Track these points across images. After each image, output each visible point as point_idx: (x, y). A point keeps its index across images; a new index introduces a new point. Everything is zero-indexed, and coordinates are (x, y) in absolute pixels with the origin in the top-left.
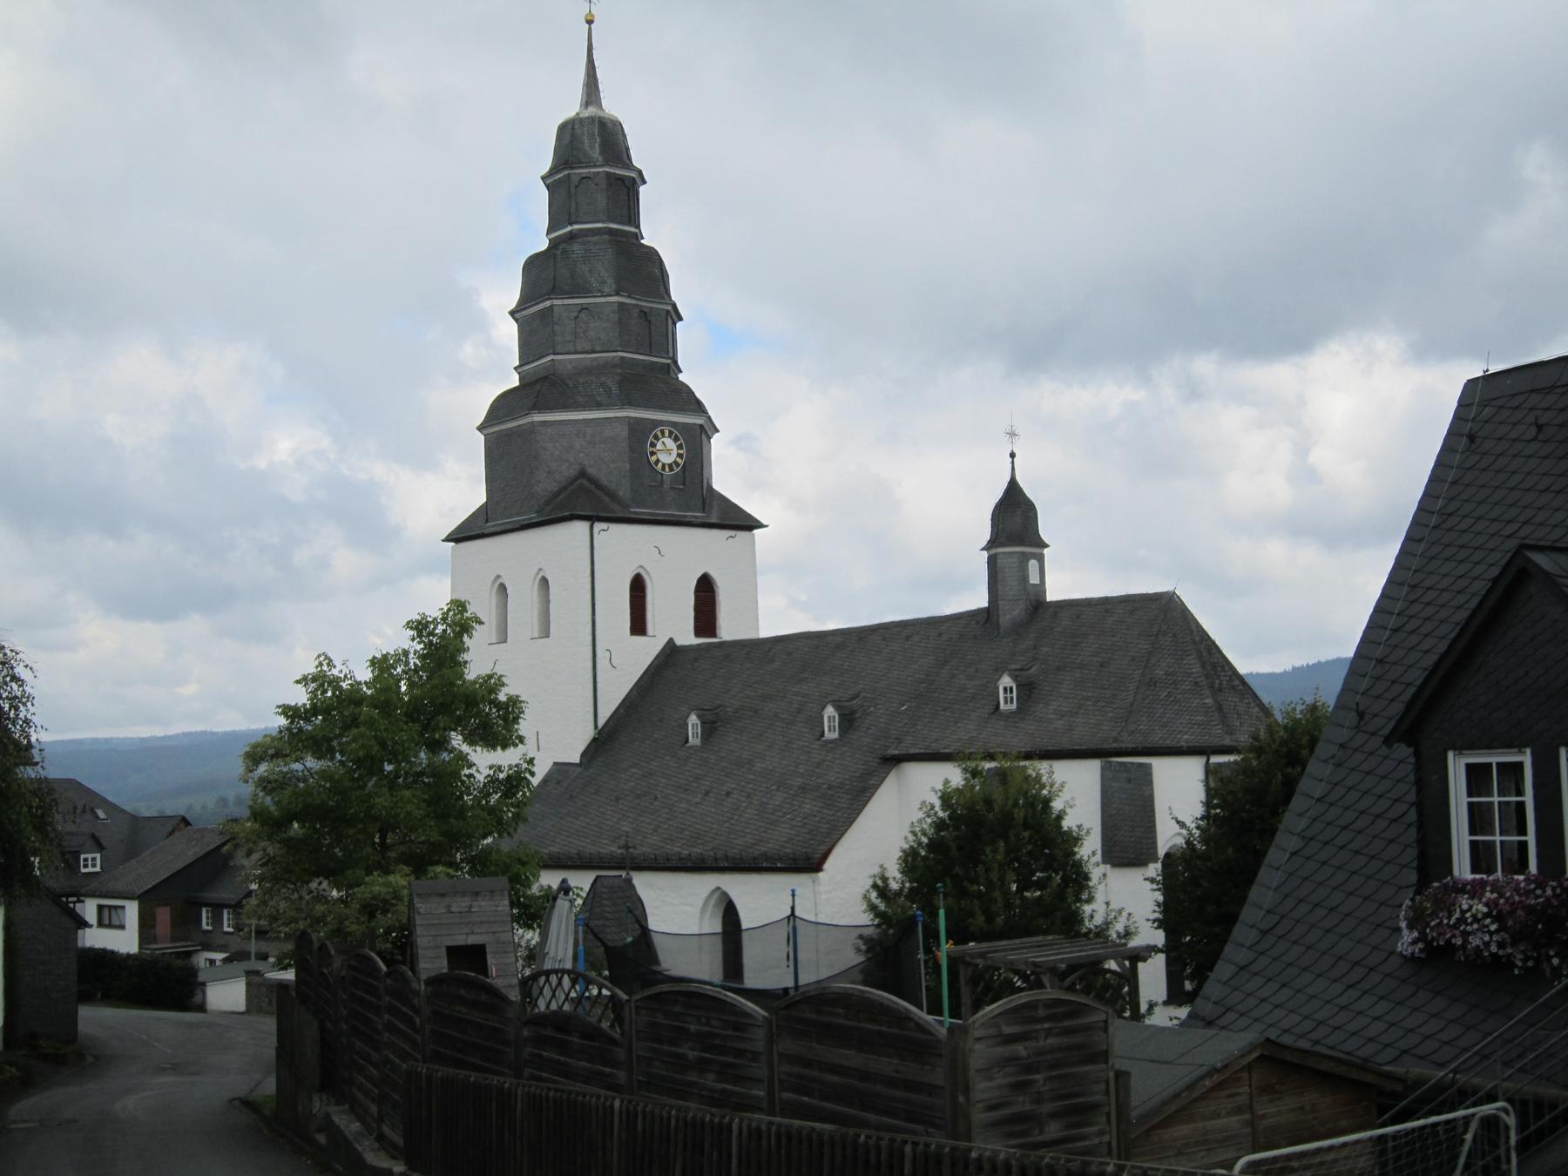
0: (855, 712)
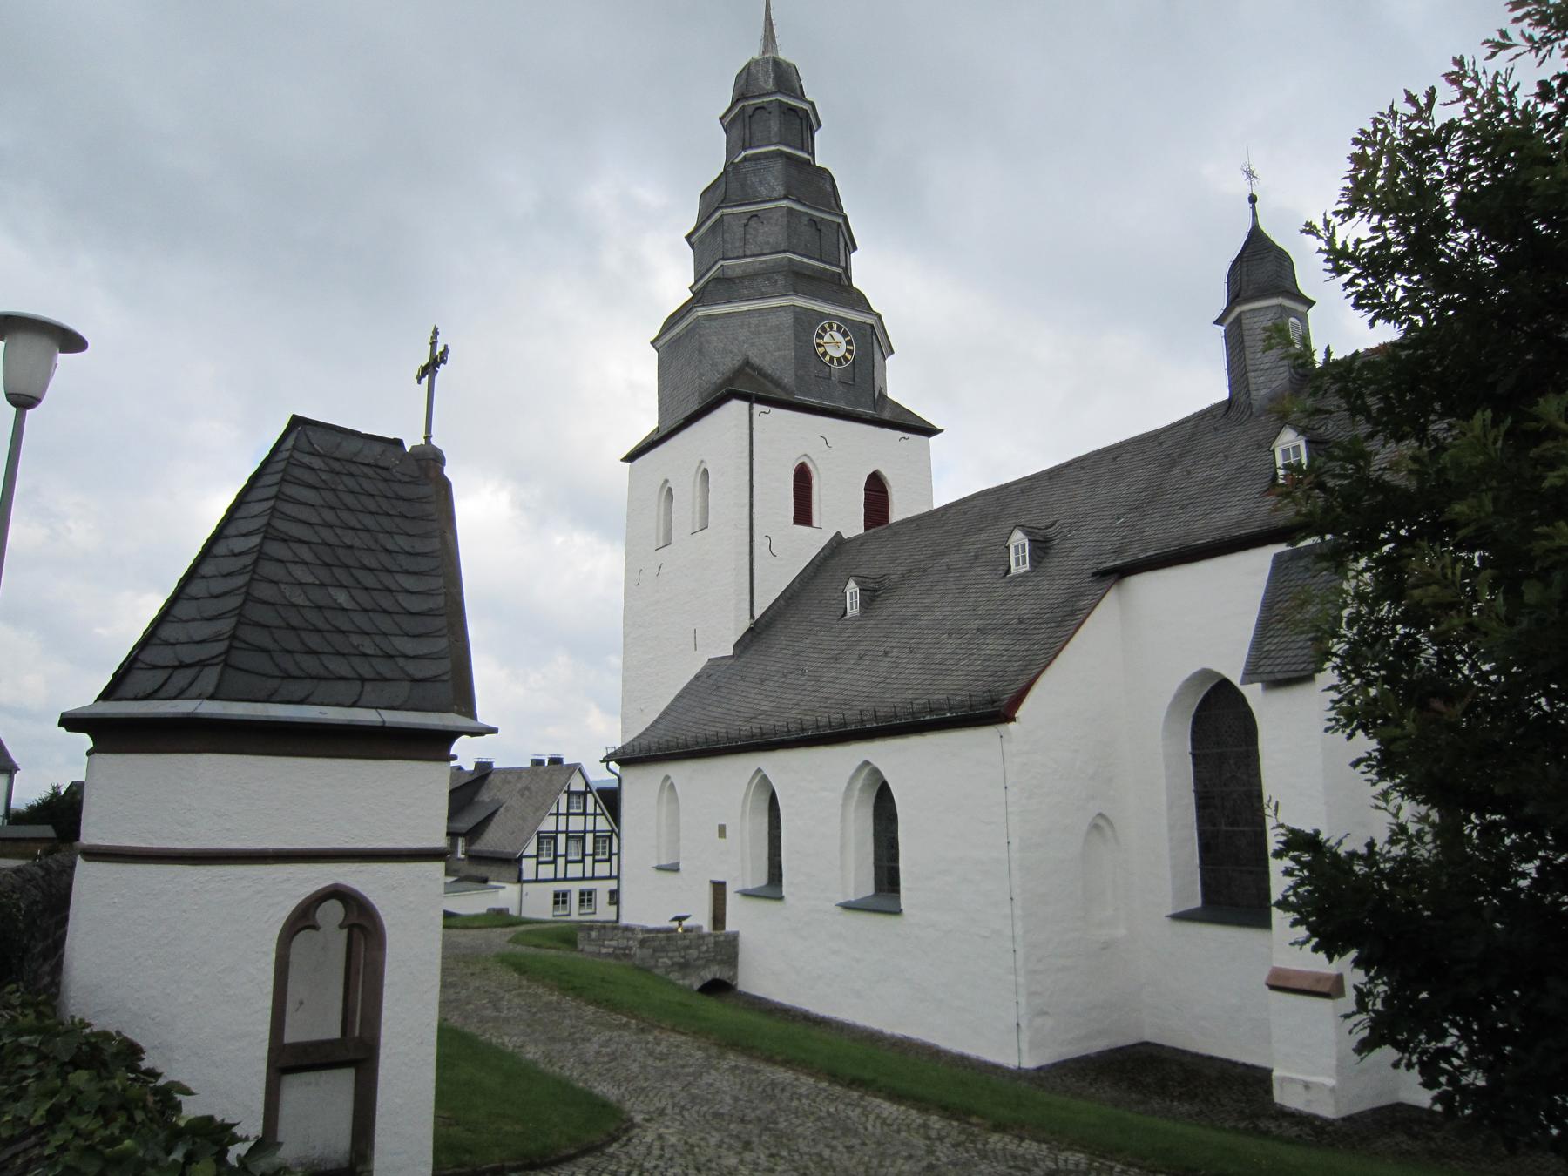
0: (1051, 540)
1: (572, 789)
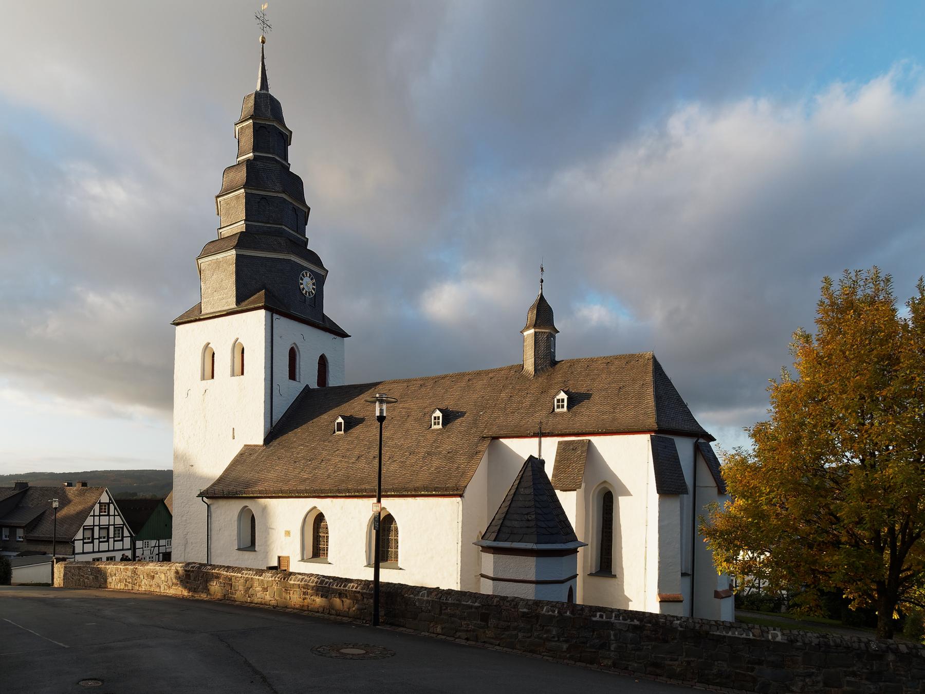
1: (101, 502)
